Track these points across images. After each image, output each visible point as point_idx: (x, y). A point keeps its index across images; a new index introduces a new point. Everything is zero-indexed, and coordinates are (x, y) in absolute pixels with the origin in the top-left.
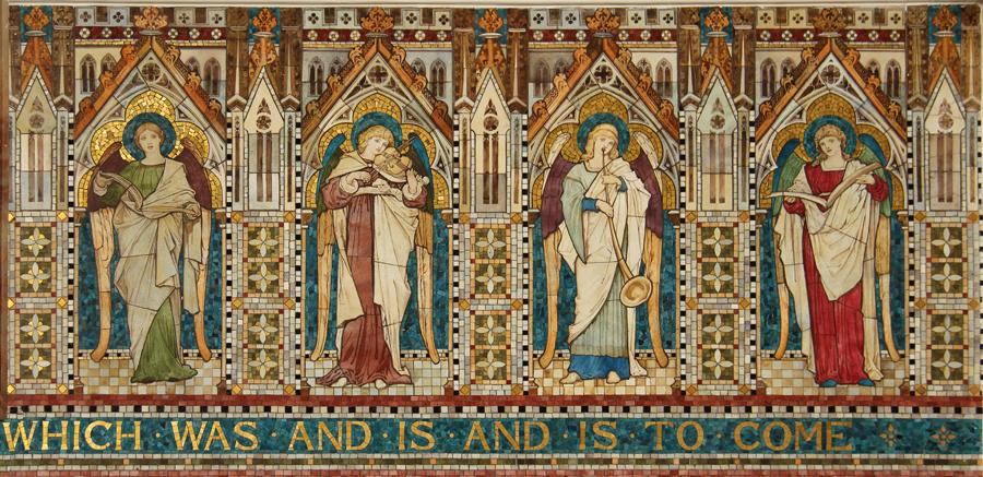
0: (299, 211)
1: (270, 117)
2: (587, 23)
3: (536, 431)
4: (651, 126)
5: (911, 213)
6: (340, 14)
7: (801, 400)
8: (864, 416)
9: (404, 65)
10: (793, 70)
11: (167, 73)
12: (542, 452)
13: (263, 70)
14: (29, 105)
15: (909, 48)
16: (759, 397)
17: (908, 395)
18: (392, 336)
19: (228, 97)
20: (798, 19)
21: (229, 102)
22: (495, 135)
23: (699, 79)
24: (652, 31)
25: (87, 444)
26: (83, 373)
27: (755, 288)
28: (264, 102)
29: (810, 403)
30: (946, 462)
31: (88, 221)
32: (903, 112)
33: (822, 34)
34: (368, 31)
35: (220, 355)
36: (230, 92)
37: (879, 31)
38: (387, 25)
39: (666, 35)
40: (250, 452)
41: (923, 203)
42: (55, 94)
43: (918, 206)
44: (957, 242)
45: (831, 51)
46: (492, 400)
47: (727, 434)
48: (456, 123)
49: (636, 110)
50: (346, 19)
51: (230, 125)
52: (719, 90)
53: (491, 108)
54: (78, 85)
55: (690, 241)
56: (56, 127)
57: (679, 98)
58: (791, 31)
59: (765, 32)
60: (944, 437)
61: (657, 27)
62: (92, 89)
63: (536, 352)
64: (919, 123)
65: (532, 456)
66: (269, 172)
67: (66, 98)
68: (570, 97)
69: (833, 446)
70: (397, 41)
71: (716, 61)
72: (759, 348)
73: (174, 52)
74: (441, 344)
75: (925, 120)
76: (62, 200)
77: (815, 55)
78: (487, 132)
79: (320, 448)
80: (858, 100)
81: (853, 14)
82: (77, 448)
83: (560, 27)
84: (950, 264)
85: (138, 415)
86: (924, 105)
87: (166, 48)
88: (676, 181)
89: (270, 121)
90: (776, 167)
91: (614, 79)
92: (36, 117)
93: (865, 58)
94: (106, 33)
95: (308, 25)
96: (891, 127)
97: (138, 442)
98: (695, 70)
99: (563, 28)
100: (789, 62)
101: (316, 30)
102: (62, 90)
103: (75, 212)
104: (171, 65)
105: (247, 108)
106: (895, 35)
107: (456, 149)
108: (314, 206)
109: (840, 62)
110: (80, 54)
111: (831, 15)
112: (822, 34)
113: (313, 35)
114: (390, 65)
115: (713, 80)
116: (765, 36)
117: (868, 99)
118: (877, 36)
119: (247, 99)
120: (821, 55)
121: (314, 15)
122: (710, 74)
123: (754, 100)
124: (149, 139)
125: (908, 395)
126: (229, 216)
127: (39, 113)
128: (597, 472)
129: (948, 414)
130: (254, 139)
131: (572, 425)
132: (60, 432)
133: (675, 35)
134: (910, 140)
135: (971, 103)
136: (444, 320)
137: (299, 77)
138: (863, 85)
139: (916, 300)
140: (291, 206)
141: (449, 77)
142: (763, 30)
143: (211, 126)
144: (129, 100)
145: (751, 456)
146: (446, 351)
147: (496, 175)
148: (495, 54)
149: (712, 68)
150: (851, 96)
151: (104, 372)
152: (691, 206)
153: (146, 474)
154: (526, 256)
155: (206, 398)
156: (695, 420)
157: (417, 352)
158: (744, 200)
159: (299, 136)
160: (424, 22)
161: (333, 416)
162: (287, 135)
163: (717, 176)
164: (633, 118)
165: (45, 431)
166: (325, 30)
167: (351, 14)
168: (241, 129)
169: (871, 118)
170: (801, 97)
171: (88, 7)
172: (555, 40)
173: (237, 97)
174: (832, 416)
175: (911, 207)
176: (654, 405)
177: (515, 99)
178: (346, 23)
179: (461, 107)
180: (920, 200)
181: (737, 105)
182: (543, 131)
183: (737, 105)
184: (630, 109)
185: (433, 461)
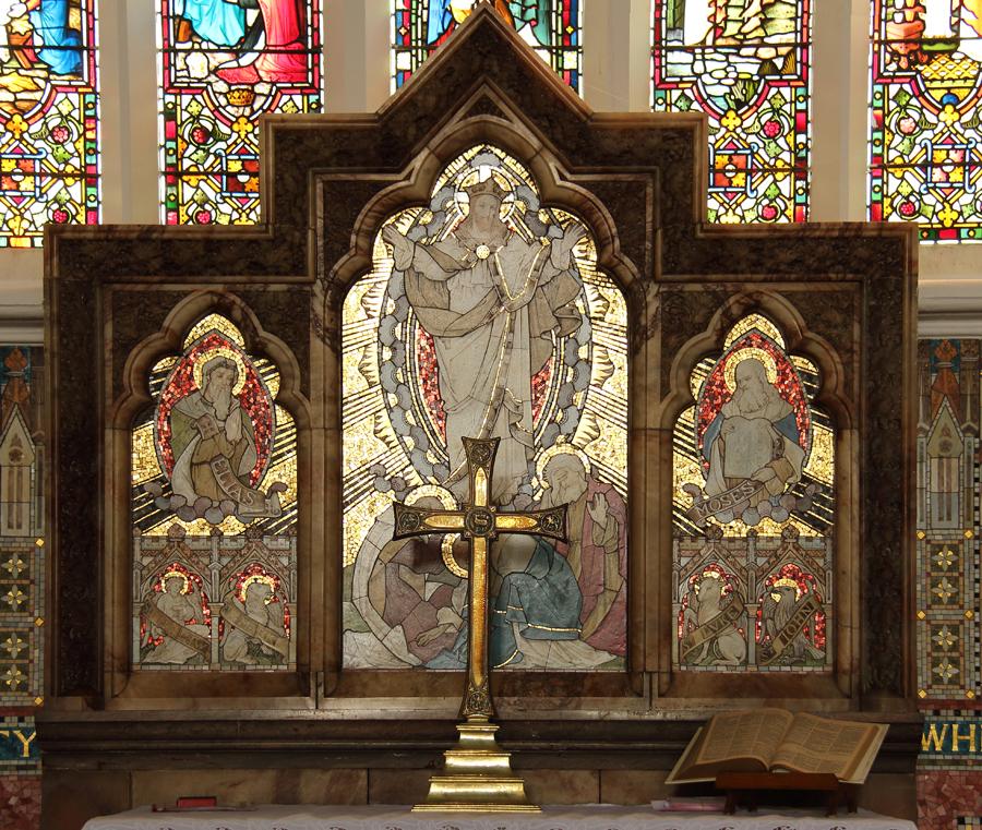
1: (951, 440)
14: (939, 430)
42: (962, 420)
53: (16, 441)
76: (969, 520)
165: (955, 733)
181: (964, 432)
183: (964, 432)
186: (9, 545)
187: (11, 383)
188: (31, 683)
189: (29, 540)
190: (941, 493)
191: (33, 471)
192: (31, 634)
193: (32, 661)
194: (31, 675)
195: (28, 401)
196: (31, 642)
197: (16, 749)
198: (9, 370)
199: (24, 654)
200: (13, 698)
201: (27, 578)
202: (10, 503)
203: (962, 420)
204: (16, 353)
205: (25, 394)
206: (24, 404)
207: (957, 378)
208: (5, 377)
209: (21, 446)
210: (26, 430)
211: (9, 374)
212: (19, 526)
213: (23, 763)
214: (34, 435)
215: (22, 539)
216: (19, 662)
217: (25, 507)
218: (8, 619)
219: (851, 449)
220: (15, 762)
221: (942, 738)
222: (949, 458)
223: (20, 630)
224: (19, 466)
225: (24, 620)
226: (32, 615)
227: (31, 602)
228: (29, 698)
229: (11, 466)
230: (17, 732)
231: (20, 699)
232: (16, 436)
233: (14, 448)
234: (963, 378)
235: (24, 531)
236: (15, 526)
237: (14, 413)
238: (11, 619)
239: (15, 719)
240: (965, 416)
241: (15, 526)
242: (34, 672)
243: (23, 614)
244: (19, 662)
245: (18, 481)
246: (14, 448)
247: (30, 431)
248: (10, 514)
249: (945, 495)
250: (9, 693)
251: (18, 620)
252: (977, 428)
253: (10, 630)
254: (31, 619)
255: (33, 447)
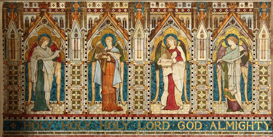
0: (149, 61)
1: (266, 34)
2: (228, 7)
3: (166, 124)
4: (121, 37)
5: (130, 61)
6: (33, 4)
7: (99, 115)
8: (18, 120)
9: (240, 19)
10: (97, 21)
11: (175, 22)
12: (200, 130)
13: (202, 20)
14: (137, 31)
15: (192, 14)
16: (150, 115)
17: (65, 114)
18: (48, 96)
19: (192, 28)
20: (35, 5)
21: (67, 29)
22: (14, 39)
23: (259, 24)
24: (121, 9)
25: (187, 128)
26: (152, 108)
27: (212, 84)
28: (76, 29)
29: (167, 116)
30: (81, 133)
31: (91, 65)
32: (65, 33)
33: (230, 10)
34: (105, 9)
35: (64, 102)
36: (66, 27)
37: (58, 9)
38: (236, 7)
39: (125, 10)
40: (244, 130)
41: (133, 59)
42: (18, 27)
43: (132, 60)
44: (73, 70)
45: (171, 15)
46: (141, 116)
47: (203, 126)
48: (192, 35)
49: (242, 32)
50: (35, 5)
51: (254, 37)
52: (202, 27)
53: (264, 32)
54: (213, 25)
55: (132, 69)
56: (18, 37)
57: (129, 29)
58: (51, 9)
59: (220, 9)
60: (13, 126)
61: (186, 8)
62: (92, 27)
63: (89, 102)
64: (132, 35)
65: (196, 131)
66: (75, 50)
67: (147, 29)
68: (223, 29)
69: (197, 128)
70: (238, 12)
71: (264, 18)
72: (87, 101)
73: (50, 16)
74: (189, 100)
75: (197, 35)
76: (21, 58)
77: (228, 16)
78: (12, 38)
79: (236, 129)
80: (240, 29)
81: (177, 4)
82: (236, 129)
83: (32, 8)
84: (264, 76)
85: (219, 120)
86: (196, 31)
87: (236, 15)
88: (191, 52)
89: (265, 35)
90: (248, 49)
91: (47, 23)
92: (76, 34)
93: (117, 17)
94: (221, 10)
95: (25, 7)
96: (125, 37)
97: (253, 127)
98: (7, 20)
99: (240, 8)
100: (96, 18)
101: (90, 9)
102: (146, 27)
103: (150, 62)
104: (238, 20)
105: (197, 31)
106: (245, 10)
107: (254, 42)
108: (27, 60)
109: (173, 18)
110: (25, 17)
111: (233, 4)
112: (230, 10)
113: (26, 10)
114: (174, 19)
115: (263, 23)
116: (251, 10)
117: (181, 29)
118: (222, 10)
119: (135, 28)
120: (168, 16)
121: (35, 4)
122: (74, 21)
123: (86, 29)
124: (109, 41)
125: (65, 114)
126: (192, 62)
127: (264, 34)
128: (164, 136)
129: (54, 119)
130: (199, 41)
131: (176, 123)
132: (257, 123)
133: (192, 10)
134: (130, 40)
135: (5, 30)
136: (126, 91)
137: (86, 23)
138: (179, 25)
139: (68, 86)
140: (147, 60)
141: (252, 22)
142: (152, 8)
143: (249, 37)
144: (165, 30)
145: (150, 131)
146: (64, 101)
147: (77, 50)
148: (77, 15)
149: (11, 20)
150: (239, 28)
151: (220, 108)
152: (195, 60)
153: (97, 136)
154: (149, 73)
155: (233, 115)
156: (151, 121)
157: (54, 102)
158: (209, 58)
159: (212, 39)
160: (93, 6)
161: (231, 120)
162: (146, 39)
163: (263, 51)
164: (53, 34)
165: (247, 124)
166: (30, 8)
167: (37, 4)
168: (6, 38)
169: (120, 35)
170: (225, 28)
171: (27, 2)
172: (157, 11)
173: (68, 28)
174: (144, 120)
175: (130, 60)
176: (175, 117)
177: (20, 28)
178: (35, 6)
179: (255, 31)
180: (257, 58)
181: (208, 31)
182: (123, 37)
183: (19, 31)
184: (52, 31)
185: (238, 133)
186: (262, 64)
187: (263, 13)
188: (268, 107)
189: (267, 62)
190: (203, 50)
191: (269, 41)
192: (268, 92)
193: (268, 100)
194: (268, 104)
195: (267, 19)
196: (268, 94)
197: (264, 127)
198: (262, 9)
199: (266, 98)
200: (263, 112)
201: (267, 74)
202: (262, 51)
203: (144, 28)
204: (264, 4)
205: (266, 17)
206: (266, 19)
207: (143, 14)
208: (261, 11)
209: (265, 33)
210: (267, 28)
211: (262, 10)
212: (265, 58)
213: (266, 132)
214: (269, 30)
215: (266, 62)
216: (265, 100)
217: (266, 52)
218: (262, 87)
219: (132, 37)
220: (264, 131)
221: (227, 124)
222: (140, 39)
223: (265, 90)
224: (265, 39)
225: (266, 87)
226: (268, 86)
227: (268, 82)
228: (268, 112)
229: (263, 39)
230: (265, 122)
231: (265, 112)
232: (264, 30)
233: (263, 33)
234: (18, 14)
235: (266, 60)
236: (139, 58)
237: (263, 23)
238: (262, 87)
239: (264, 118)
240: (131, 26)
241: (139, 58)
242: (269, 104)
243: (266, 86)
244: (265, 100)
245: (264, 44)
246: (12, 34)
247: (268, 28)
248: (262, 54)
249: (264, 50)
250: (262, 110)
251: (264, 87)
252: (211, 29)
253: (262, 90)
254: (268, 87)
255: (269, 33)
